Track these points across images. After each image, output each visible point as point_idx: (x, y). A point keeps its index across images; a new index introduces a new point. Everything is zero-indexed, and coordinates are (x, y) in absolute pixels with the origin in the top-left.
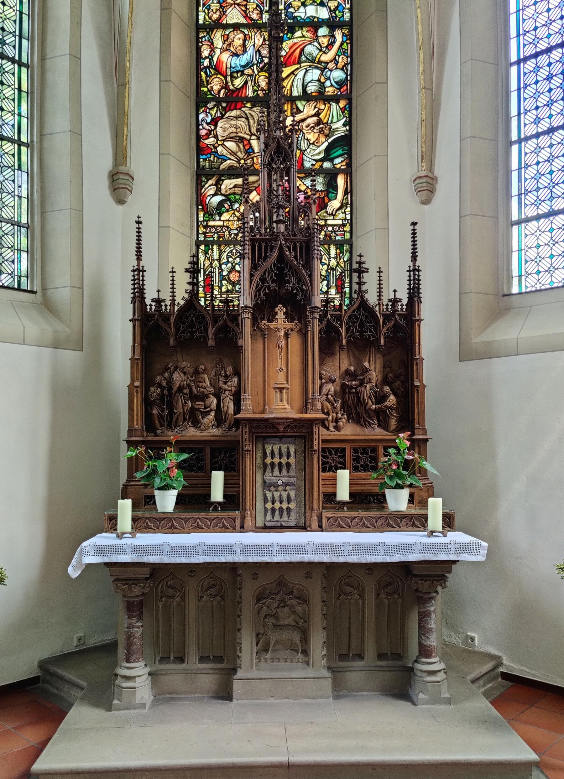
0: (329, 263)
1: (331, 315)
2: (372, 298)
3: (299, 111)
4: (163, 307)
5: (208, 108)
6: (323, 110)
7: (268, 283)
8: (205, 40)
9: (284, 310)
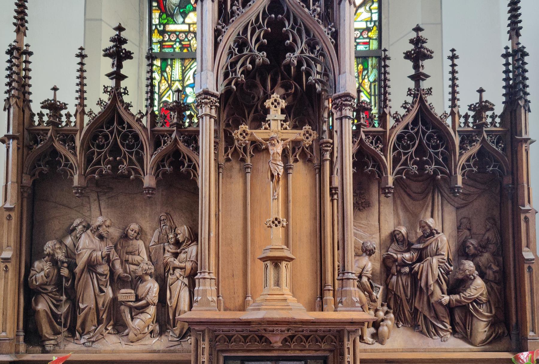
1: (367, 133)
2: (439, 104)
4: (64, 119)
7: (251, 51)
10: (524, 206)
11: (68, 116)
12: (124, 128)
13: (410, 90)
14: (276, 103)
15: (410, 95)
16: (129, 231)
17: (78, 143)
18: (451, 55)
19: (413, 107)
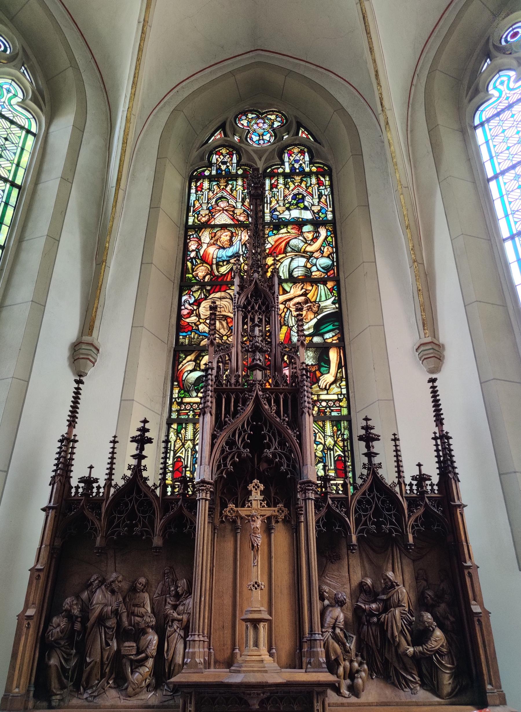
0: (325, 442)
2: (388, 475)
3: (285, 292)
4: (95, 490)
5: (191, 291)
6: (311, 290)
7: (238, 448)
8: (193, 237)
9: (262, 487)
10: (466, 563)
11: (99, 487)
12: (141, 497)
13: (364, 464)
14: (257, 487)
15: (365, 468)
16: (138, 584)
17: (103, 510)
18: (393, 438)
19: (368, 478)
